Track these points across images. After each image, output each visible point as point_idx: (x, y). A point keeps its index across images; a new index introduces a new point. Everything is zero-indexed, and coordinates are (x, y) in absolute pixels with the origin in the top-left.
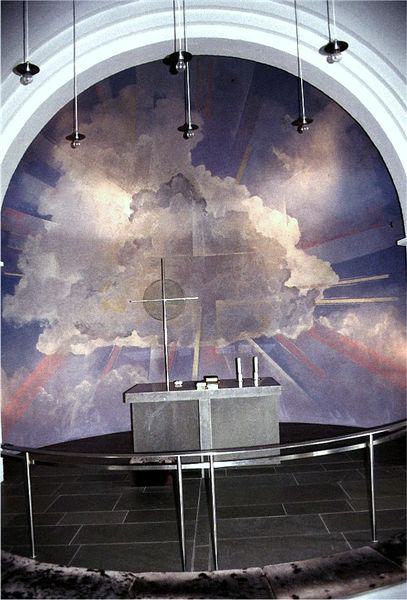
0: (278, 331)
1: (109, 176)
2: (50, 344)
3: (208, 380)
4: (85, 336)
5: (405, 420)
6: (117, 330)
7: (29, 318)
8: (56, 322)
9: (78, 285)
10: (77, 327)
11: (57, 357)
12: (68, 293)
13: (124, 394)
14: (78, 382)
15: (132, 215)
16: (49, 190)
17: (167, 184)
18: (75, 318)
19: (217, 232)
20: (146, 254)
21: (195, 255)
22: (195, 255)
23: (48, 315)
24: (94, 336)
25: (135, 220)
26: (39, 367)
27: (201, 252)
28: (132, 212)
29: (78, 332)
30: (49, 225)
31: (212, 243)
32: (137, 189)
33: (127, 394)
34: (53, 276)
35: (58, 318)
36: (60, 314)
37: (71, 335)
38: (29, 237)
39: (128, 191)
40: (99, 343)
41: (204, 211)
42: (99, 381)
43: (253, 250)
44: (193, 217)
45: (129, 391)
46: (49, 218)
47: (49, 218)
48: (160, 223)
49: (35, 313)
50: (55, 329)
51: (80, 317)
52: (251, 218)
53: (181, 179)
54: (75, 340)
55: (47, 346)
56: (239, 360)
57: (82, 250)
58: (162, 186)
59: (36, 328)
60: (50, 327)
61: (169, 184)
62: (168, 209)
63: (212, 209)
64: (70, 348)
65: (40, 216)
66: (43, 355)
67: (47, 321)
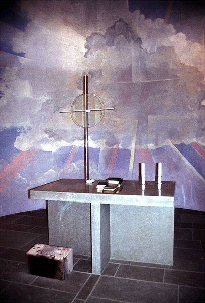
0: (194, 140)
1: (67, 23)
2: (25, 144)
3: (110, 182)
4: (52, 139)
5: (140, 165)
6: (75, 135)
7: (8, 125)
8: (30, 129)
9: (48, 102)
10: (46, 132)
11: (30, 152)
12: (39, 108)
13: (29, 191)
14: (46, 170)
15: (86, 53)
16: (21, 34)
17: (111, 28)
18: (44, 126)
19: (151, 64)
20: (98, 82)
21: (134, 81)
22: (134, 81)
23: (26, 123)
24: (59, 139)
25: (90, 56)
26: (16, 159)
27: (138, 79)
28: (86, 50)
29: (47, 136)
30: (23, 60)
31: (147, 73)
32: (89, 33)
33: (32, 192)
34: (28, 96)
35: (31, 126)
36: (33, 123)
37: (41, 137)
38: (7, 68)
39: (82, 34)
40: (63, 144)
41: (141, 48)
42: (62, 170)
43: (178, 77)
44: (131, 53)
45: (35, 189)
46: (22, 54)
47: (22, 54)
48: (107, 58)
49: (13, 123)
50: (29, 133)
51: (49, 126)
52: (176, 51)
53: (123, 24)
54: (45, 141)
55: (23, 144)
56: (160, 165)
57: (51, 78)
58: (108, 30)
59: (13, 133)
60: (25, 132)
61: (113, 27)
62: (113, 47)
63: (146, 45)
64: (41, 147)
65: (16, 54)
66: (18, 151)
67: (22, 127)
